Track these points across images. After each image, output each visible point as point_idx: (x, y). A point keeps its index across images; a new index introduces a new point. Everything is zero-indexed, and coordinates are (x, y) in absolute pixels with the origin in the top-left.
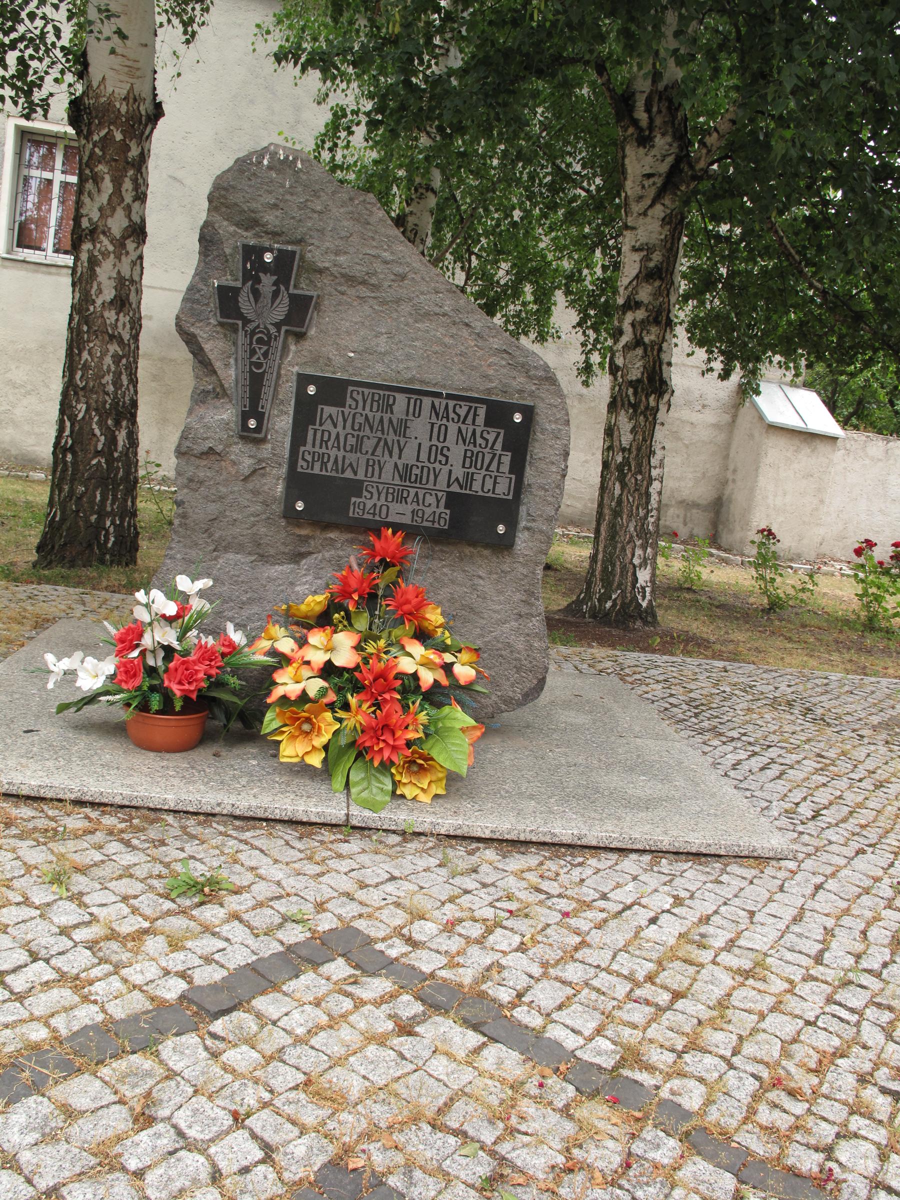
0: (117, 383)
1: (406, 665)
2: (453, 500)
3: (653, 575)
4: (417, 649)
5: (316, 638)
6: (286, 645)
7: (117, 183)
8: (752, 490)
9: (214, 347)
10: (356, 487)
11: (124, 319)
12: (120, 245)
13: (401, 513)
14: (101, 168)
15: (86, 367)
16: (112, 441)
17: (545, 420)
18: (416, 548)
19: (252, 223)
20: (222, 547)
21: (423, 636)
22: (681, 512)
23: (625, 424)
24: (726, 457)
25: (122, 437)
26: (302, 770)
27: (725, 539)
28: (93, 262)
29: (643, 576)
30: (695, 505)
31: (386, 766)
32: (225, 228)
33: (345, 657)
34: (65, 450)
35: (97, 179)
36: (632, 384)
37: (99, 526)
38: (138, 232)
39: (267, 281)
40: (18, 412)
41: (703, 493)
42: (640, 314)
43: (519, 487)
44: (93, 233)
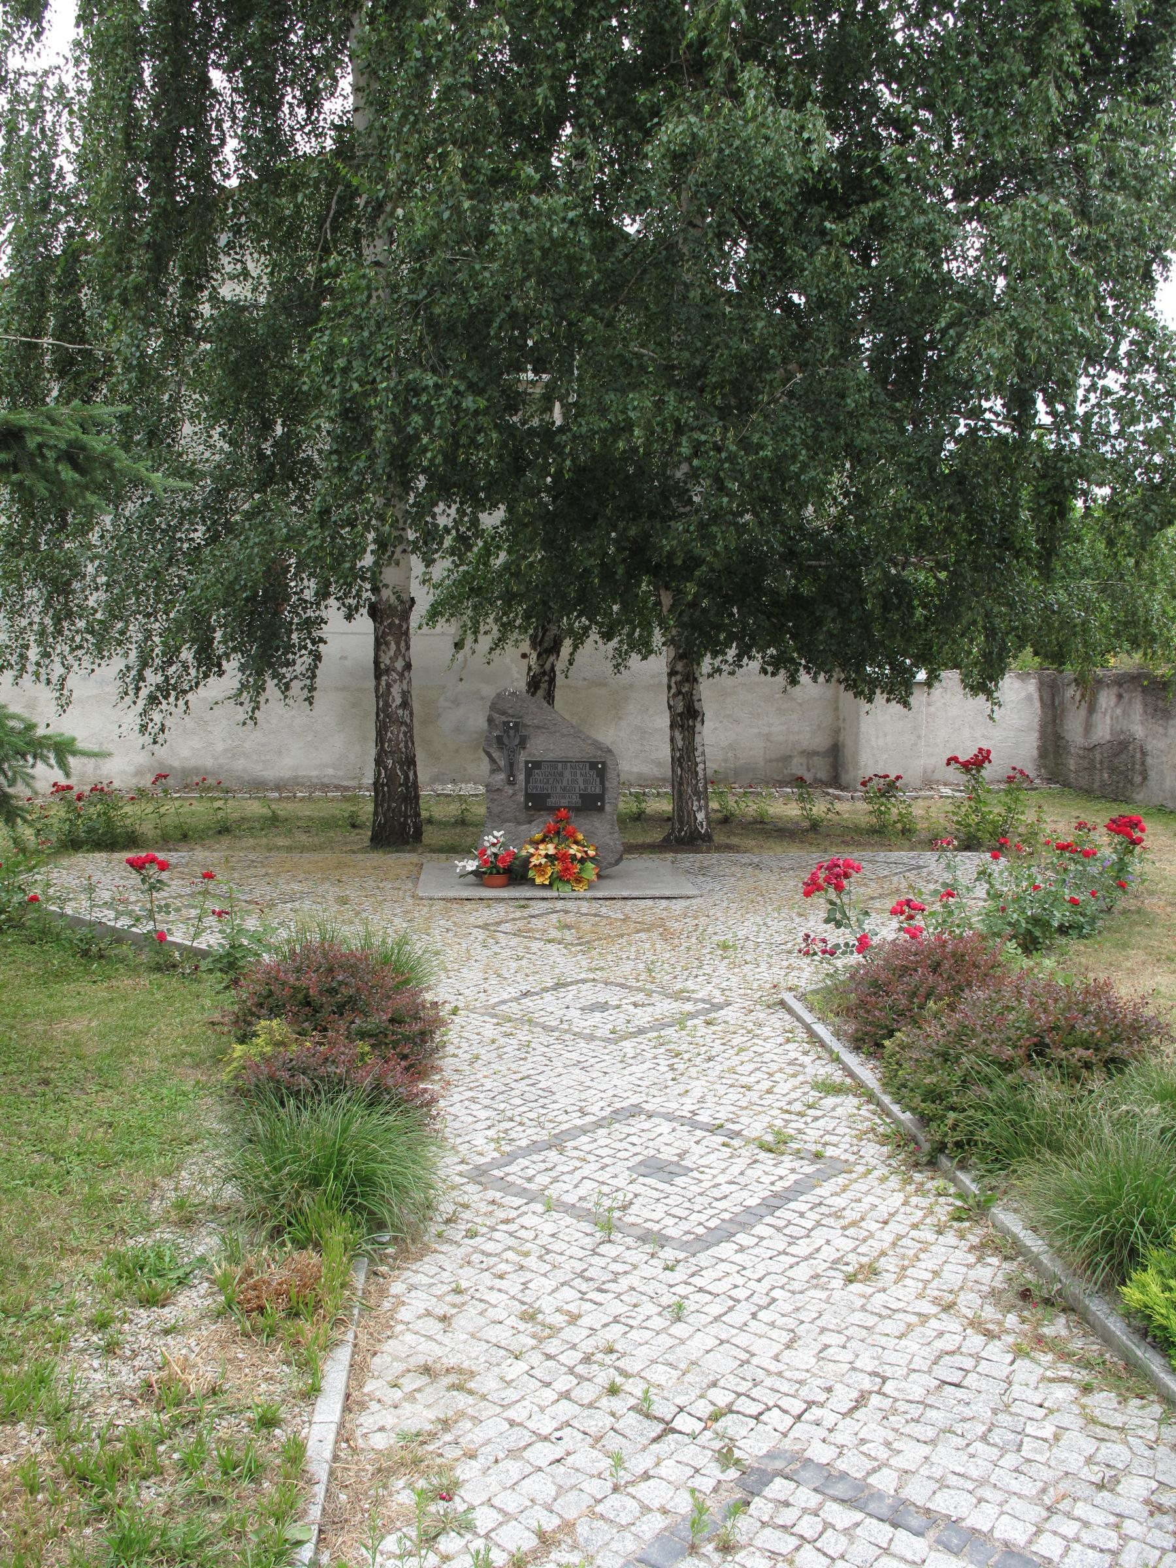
0: (406, 747)
1: (572, 852)
2: (581, 796)
3: (707, 814)
4: (575, 847)
5: (541, 847)
6: (532, 850)
7: (398, 644)
8: (857, 735)
9: (495, 755)
10: (548, 796)
11: (407, 712)
12: (402, 675)
13: (564, 802)
14: (389, 638)
15: (390, 740)
16: (407, 777)
17: (609, 763)
18: (572, 814)
19: (504, 713)
20: (504, 821)
21: (576, 842)
22: (804, 760)
23: (678, 736)
24: (836, 709)
25: (411, 774)
26: (543, 886)
27: (845, 778)
28: (389, 686)
29: (701, 816)
30: (815, 753)
31: (568, 881)
32: (496, 716)
33: (552, 851)
34: (383, 785)
35: (387, 644)
36: (680, 715)
37: (405, 824)
38: (408, 666)
39: (512, 732)
40: (247, 745)
41: (821, 742)
42: (679, 678)
43: (604, 789)
44: (387, 671)
